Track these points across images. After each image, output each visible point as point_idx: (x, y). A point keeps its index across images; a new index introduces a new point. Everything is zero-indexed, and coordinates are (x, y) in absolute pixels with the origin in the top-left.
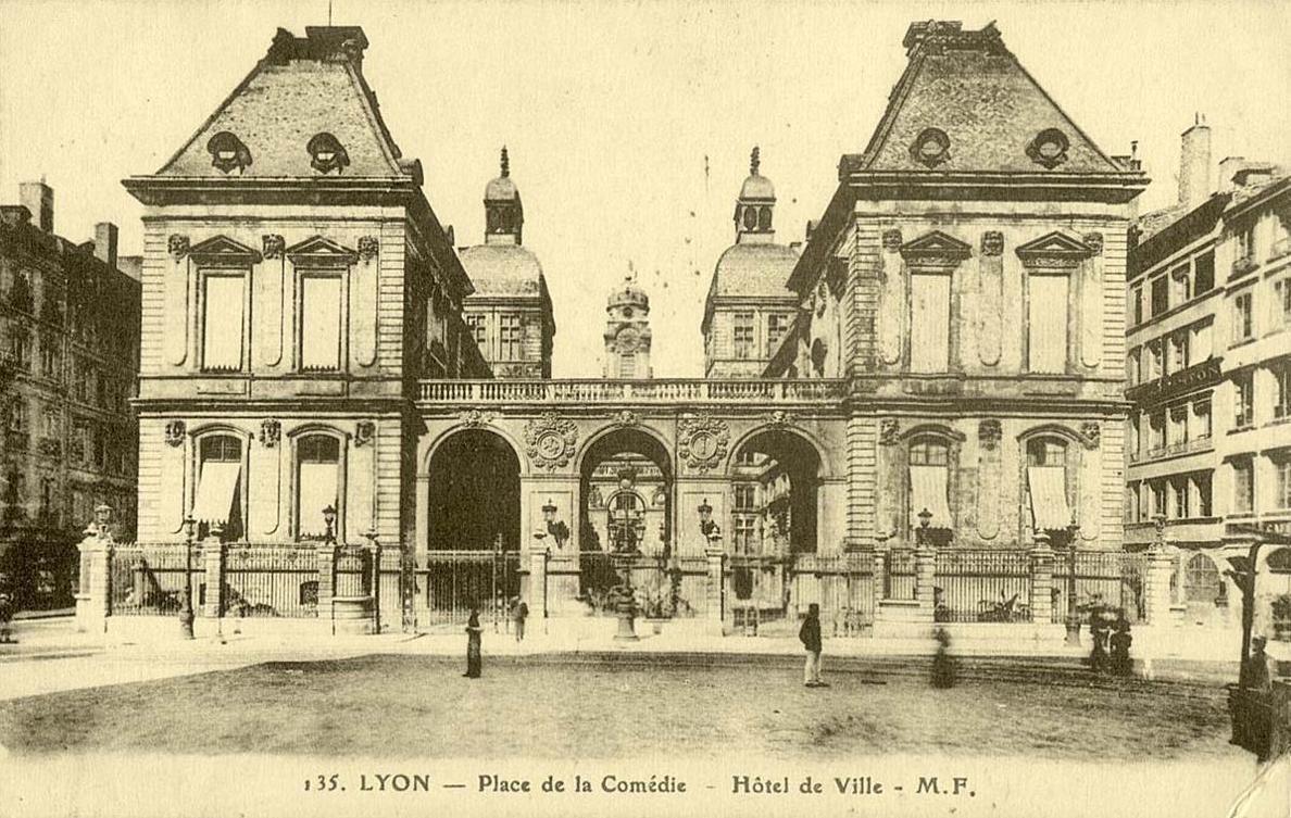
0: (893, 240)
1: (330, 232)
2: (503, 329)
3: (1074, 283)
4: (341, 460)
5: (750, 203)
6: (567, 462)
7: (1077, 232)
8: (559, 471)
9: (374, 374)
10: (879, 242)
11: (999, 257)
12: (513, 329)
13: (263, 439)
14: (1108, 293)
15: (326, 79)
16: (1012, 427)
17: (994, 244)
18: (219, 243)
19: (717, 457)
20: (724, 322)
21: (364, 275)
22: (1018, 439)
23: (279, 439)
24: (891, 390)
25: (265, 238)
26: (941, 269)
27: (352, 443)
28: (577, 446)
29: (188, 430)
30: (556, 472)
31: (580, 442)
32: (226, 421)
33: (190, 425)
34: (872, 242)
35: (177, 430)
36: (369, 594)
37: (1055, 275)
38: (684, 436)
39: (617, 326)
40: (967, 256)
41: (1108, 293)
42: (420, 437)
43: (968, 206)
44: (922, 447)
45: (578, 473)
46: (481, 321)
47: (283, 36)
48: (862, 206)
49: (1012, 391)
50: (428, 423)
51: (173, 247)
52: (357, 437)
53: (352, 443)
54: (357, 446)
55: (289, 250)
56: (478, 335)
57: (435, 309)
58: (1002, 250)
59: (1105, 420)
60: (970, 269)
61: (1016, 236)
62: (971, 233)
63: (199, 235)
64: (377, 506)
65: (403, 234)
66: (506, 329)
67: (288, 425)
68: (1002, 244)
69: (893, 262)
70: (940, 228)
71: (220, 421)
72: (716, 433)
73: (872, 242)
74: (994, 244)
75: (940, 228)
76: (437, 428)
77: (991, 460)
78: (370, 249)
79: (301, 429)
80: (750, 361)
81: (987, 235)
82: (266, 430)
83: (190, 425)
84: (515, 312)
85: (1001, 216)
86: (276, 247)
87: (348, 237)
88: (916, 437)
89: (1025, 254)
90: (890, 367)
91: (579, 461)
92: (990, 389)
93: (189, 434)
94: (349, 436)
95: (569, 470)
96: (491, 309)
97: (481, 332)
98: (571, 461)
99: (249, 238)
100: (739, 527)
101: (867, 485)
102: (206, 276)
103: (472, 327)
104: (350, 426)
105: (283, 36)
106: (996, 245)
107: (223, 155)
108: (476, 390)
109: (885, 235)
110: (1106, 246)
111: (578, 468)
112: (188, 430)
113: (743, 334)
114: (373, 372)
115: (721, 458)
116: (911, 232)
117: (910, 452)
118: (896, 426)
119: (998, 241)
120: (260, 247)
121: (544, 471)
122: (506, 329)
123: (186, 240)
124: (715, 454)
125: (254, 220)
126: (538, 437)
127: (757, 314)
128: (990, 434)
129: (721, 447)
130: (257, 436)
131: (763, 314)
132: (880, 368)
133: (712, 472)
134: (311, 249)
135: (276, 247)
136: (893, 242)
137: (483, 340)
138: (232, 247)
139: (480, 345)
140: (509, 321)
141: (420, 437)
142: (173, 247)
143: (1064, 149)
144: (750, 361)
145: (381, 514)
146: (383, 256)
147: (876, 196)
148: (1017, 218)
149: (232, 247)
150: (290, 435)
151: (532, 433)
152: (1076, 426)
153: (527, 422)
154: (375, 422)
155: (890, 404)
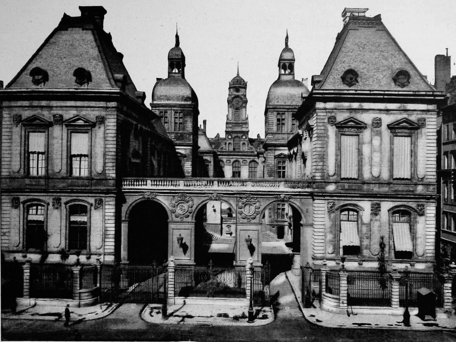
0: (332, 121)
1: (84, 113)
2: (175, 118)
3: (413, 139)
4: (89, 213)
5: (284, 62)
6: (189, 215)
7: (414, 118)
8: (185, 219)
9: (103, 178)
10: (326, 121)
11: (380, 128)
12: (180, 118)
13: (53, 205)
14: (428, 145)
15: (84, 38)
16: (386, 206)
17: (377, 123)
18: (34, 118)
19: (255, 214)
20: (273, 118)
21: (99, 132)
22: (389, 211)
23: (61, 206)
24: (331, 188)
25: (54, 116)
26: (354, 133)
27: (93, 208)
28: (194, 208)
29: (21, 200)
30: (184, 220)
31: (195, 207)
32: (37, 197)
33: (22, 198)
34: (322, 121)
35: (17, 202)
36: (96, 286)
37: (405, 136)
38: (240, 204)
39: (233, 96)
40: (365, 128)
41: (428, 145)
42: (123, 205)
43: (366, 105)
44: (346, 213)
45: (194, 221)
46: (166, 114)
47: (66, 17)
48: (320, 105)
49: (385, 189)
50: (127, 197)
51: (15, 120)
52: (95, 205)
53: (93, 208)
54: (95, 209)
55: (65, 122)
56: (164, 120)
57: (135, 133)
58: (381, 125)
59: (427, 202)
60: (366, 134)
61: (387, 119)
62: (367, 118)
63: (26, 114)
64: (105, 236)
65: (116, 114)
66: (177, 118)
67: (64, 200)
68: (381, 123)
69: (332, 131)
70: (353, 115)
71: (35, 197)
72: (254, 204)
73: (322, 121)
74: (377, 123)
75: (353, 115)
76: (131, 200)
77: (376, 220)
78: (102, 120)
79: (71, 201)
80: (284, 134)
81: (374, 119)
82: (55, 201)
83: (22, 198)
84: (181, 110)
85: (380, 110)
86: (59, 120)
87: (92, 115)
88: (343, 209)
89: (391, 127)
90: (331, 178)
91: (194, 215)
92: (376, 189)
93: (22, 203)
94: (92, 205)
95: (189, 219)
96: (170, 109)
97: (165, 119)
98: (191, 215)
99: (47, 115)
100: (279, 207)
101: (316, 241)
102: (29, 132)
103: (162, 117)
104: (92, 200)
105: (66, 17)
106: (378, 123)
107: (36, 77)
108: (149, 182)
109: (329, 118)
110: (427, 123)
111: (194, 218)
112: (21, 200)
113: (280, 123)
114: (102, 177)
115: (257, 215)
116: (341, 117)
117: (340, 215)
118: (334, 204)
119: (379, 121)
120: (52, 120)
121: (178, 219)
122: (177, 118)
123: (20, 116)
124: (254, 213)
125: (50, 108)
126: (176, 204)
127: (286, 113)
128: (376, 210)
129: (257, 210)
130: (51, 204)
131: (289, 113)
132: (327, 178)
133: (253, 221)
134: (75, 121)
135: (59, 120)
136: (332, 121)
137: (166, 123)
138: (39, 120)
139: (166, 124)
140: (178, 114)
141: (123, 205)
142: (15, 120)
143: (408, 79)
144: (284, 134)
145: (106, 240)
146: (107, 123)
147: (325, 100)
148: (387, 111)
149: (39, 120)
150: (66, 203)
151: (174, 202)
152: (414, 205)
153: (171, 197)
154: (103, 198)
155: (331, 195)
